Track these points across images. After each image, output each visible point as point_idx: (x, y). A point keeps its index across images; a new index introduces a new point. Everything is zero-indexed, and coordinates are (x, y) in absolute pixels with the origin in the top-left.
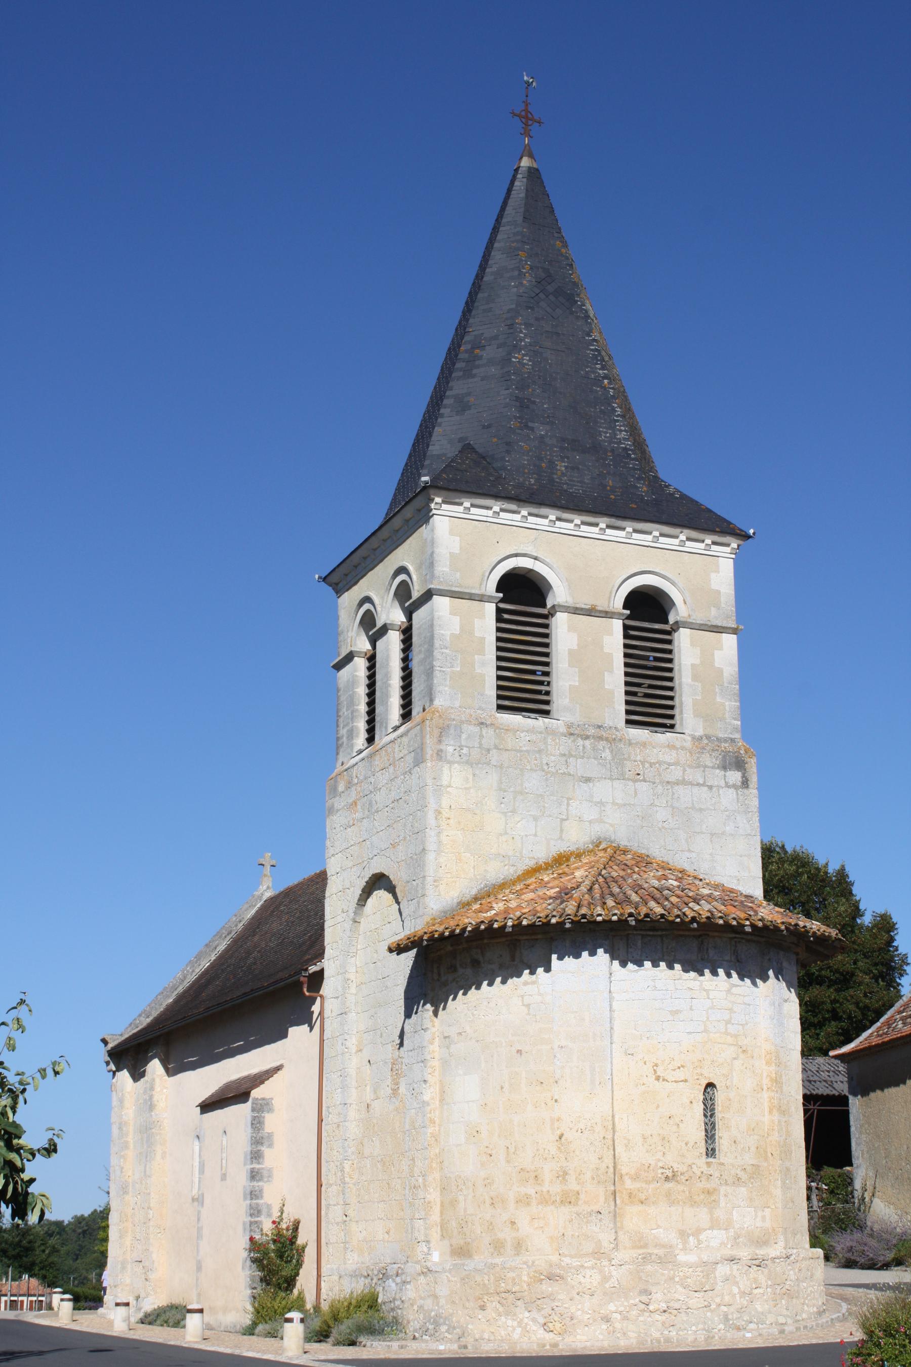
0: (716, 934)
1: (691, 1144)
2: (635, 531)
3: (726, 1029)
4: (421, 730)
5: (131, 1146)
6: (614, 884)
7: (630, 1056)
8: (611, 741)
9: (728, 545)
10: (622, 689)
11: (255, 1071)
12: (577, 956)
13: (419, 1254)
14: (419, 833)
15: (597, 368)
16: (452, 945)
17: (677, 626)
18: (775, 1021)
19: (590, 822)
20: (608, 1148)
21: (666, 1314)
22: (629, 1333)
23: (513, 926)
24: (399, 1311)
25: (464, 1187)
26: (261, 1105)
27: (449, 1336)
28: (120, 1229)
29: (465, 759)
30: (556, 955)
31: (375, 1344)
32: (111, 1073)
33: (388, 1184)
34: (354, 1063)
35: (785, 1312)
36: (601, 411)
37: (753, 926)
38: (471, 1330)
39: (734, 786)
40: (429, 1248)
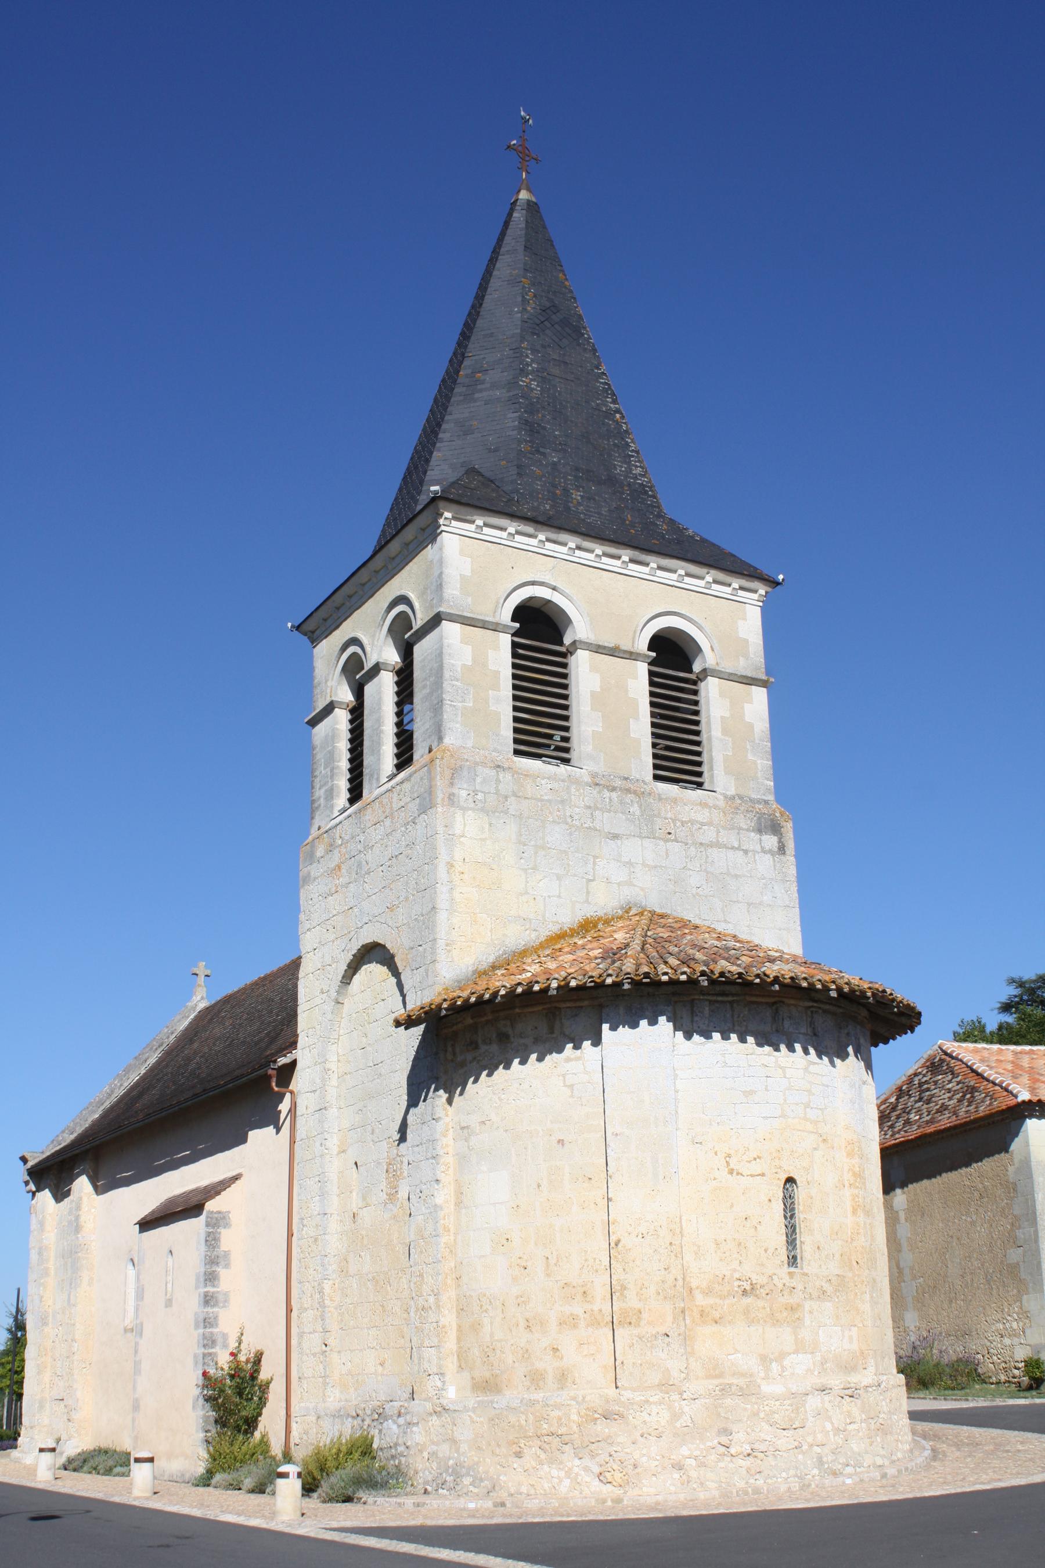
0: (792, 1002)
1: (771, 1251)
2: (660, 568)
3: (805, 1114)
4: (429, 772)
5: (52, 1272)
6: (668, 944)
7: (698, 1145)
8: (640, 795)
9: (755, 592)
10: (648, 740)
11: (204, 1183)
12: (634, 1025)
13: (430, 1389)
14: (427, 890)
15: (607, 402)
16: (472, 1018)
17: (705, 673)
18: (856, 1106)
19: (619, 884)
20: (676, 1256)
21: (751, 1459)
22: (707, 1483)
23: (559, 988)
24: (403, 1459)
25: (490, 1308)
26: (217, 1219)
27: (476, 1490)
28: (38, 1365)
29: (480, 805)
30: (608, 1025)
31: (380, 1500)
32: (31, 1194)
33: (383, 1306)
34: (335, 1167)
35: (882, 1452)
36: (615, 445)
37: (839, 990)
38: (505, 1482)
39: (770, 852)
40: (444, 1382)
